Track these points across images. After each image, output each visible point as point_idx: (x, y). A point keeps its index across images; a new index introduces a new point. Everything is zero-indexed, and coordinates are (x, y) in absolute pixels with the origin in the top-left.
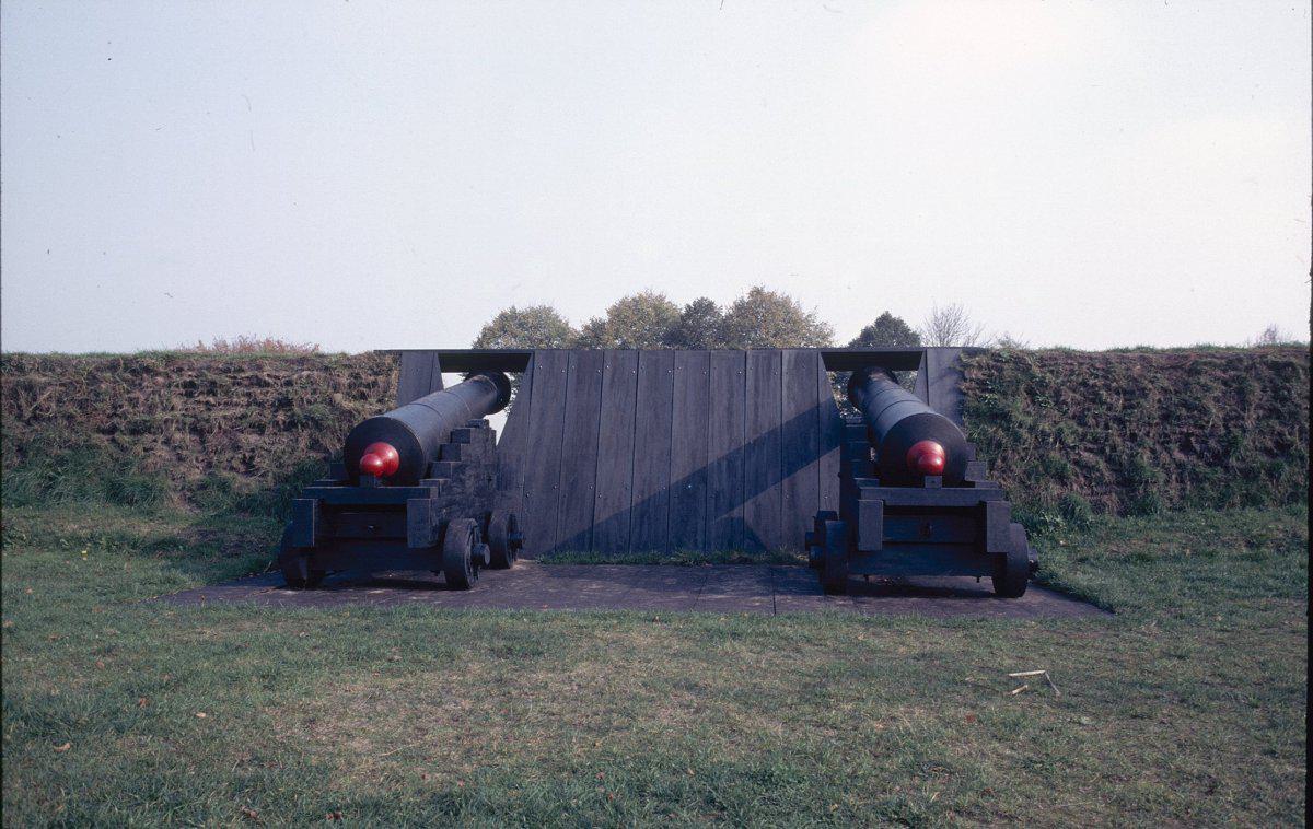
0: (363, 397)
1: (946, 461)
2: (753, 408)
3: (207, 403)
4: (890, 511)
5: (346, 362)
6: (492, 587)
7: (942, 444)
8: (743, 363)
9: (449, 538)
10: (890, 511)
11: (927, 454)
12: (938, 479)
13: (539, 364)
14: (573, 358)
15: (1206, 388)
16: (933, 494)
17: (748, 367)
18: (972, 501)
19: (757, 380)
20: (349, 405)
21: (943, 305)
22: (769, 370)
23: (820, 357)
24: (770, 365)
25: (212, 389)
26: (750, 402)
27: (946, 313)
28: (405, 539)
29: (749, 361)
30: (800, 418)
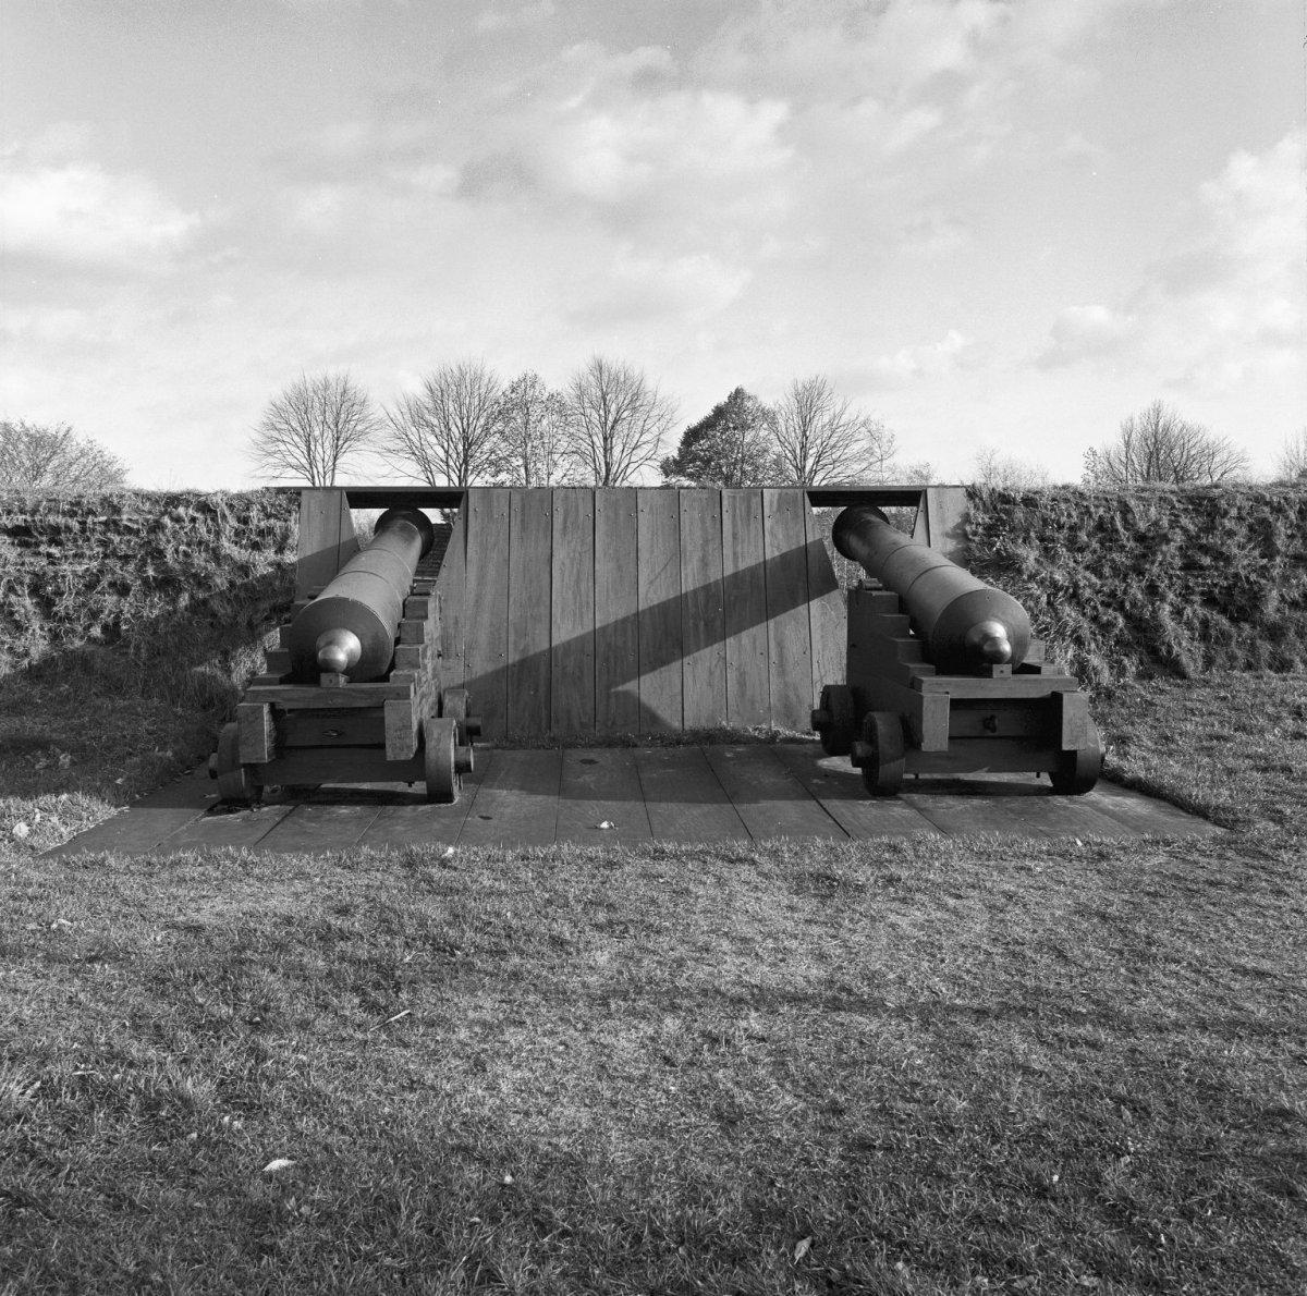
0: (256, 546)
1: (1013, 647)
2: (731, 557)
3: (49, 555)
4: (956, 704)
5: (241, 505)
6: (740, 976)
7: (1005, 623)
8: (718, 505)
9: (430, 745)
10: (956, 704)
11: (990, 639)
12: (1007, 668)
13: (473, 500)
14: (516, 498)
15: (1231, 534)
16: (1001, 685)
17: (724, 509)
18: (1046, 692)
19: (734, 525)
20: (239, 554)
21: (804, 376)
22: (749, 513)
23: (806, 495)
24: (749, 507)
25: (55, 535)
26: (728, 551)
27: (808, 387)
28: (382, 746)
29: (725, 502)
30: (784, 558)
